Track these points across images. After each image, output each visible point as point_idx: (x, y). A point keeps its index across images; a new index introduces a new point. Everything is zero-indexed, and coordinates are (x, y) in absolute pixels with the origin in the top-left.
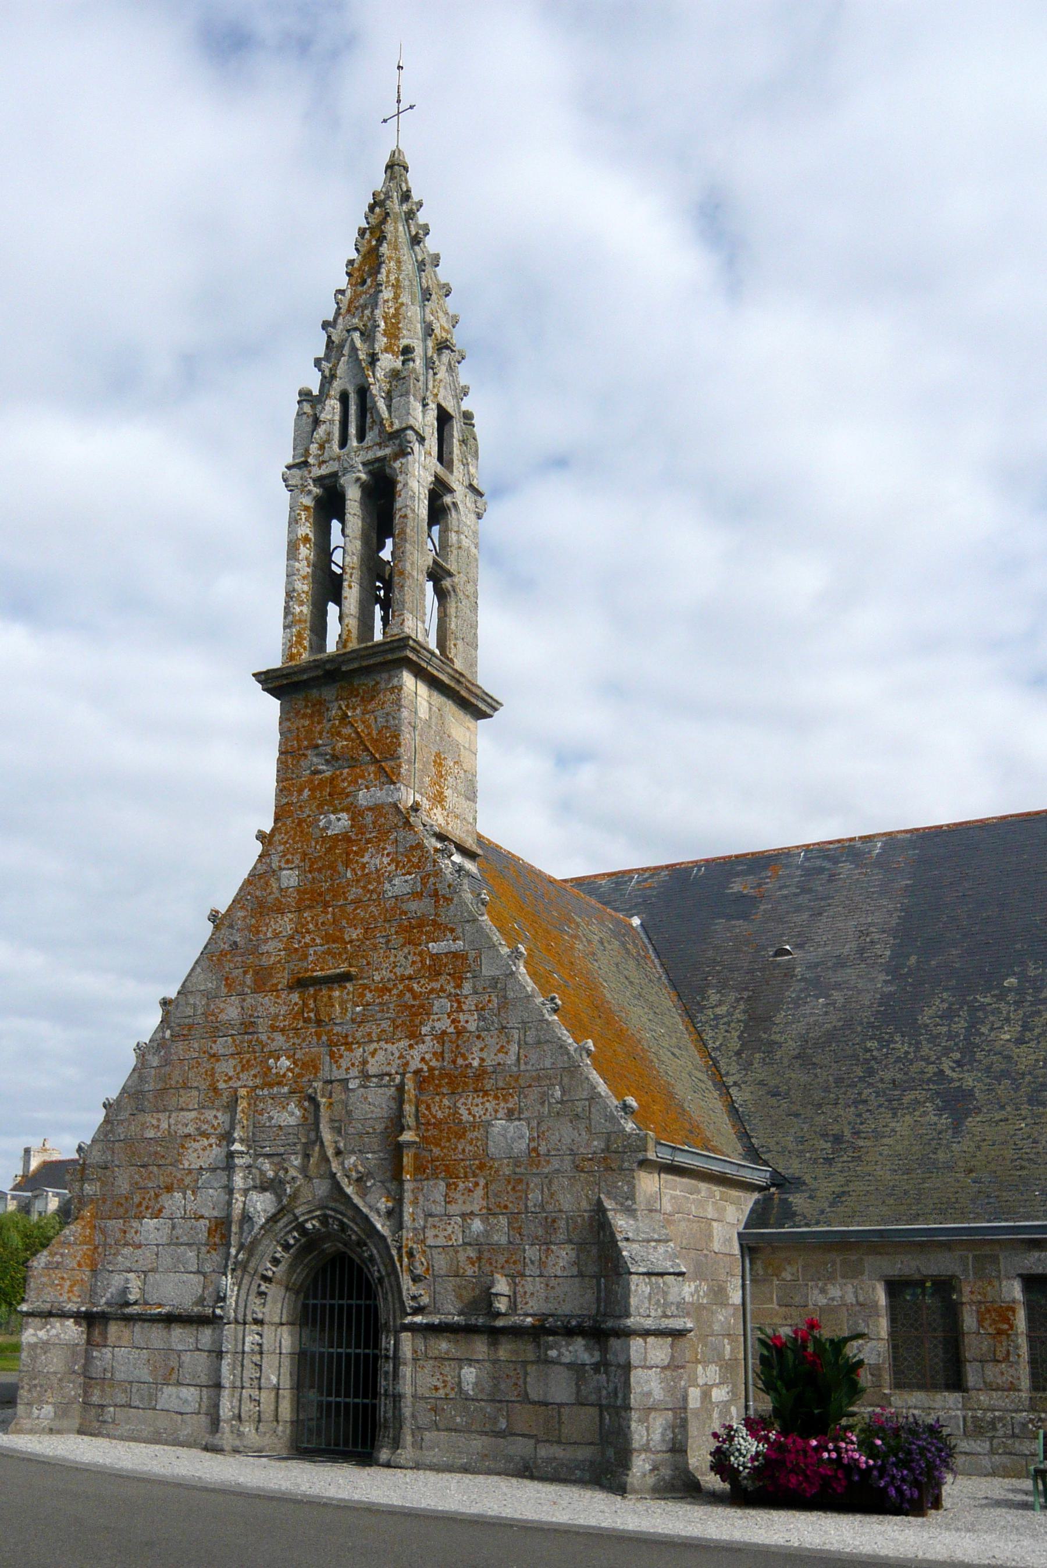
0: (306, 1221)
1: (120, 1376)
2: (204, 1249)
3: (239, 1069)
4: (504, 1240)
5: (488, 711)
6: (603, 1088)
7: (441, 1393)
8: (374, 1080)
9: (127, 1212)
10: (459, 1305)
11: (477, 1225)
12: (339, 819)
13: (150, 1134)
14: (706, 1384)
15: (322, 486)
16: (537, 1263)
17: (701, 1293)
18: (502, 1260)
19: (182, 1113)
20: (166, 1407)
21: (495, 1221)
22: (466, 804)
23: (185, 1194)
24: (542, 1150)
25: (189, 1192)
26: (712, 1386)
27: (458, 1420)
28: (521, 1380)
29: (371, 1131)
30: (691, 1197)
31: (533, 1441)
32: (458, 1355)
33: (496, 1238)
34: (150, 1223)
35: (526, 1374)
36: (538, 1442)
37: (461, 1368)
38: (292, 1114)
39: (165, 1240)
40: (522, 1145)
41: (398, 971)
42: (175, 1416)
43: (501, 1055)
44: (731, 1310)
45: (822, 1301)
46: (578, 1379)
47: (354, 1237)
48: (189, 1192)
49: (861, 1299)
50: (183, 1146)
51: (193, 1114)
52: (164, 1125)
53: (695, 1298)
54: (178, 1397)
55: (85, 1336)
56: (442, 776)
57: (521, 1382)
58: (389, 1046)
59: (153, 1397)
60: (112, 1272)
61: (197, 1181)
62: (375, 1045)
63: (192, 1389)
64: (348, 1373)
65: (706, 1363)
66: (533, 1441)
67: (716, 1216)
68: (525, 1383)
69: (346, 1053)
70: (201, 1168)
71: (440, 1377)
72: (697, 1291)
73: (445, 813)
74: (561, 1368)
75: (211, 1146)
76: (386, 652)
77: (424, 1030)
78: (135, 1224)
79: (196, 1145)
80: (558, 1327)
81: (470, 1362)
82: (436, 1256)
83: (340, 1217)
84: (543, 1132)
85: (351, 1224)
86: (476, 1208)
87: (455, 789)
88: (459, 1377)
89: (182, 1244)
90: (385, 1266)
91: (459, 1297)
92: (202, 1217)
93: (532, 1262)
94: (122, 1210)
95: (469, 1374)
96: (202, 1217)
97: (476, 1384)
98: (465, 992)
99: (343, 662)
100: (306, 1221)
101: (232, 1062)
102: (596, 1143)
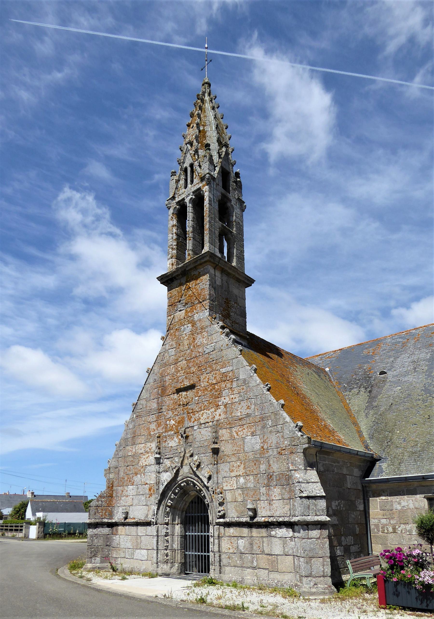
0: (182, 483)
1: (122, 546)
2: (148, 496)
3: (157, 426)
4: (252, 486)
5: (249, 283)
6: (288, 419)
7: (231, 551)
8: (203, 425)
9: (123, 483)
10: (237, 514)
11: (242, 480)
12: (188, 327)
13: (130, 454)
14: (346, 545)
15: (179, 205)
16: (265, 495)
17: (342, 506)
18: (252, 493)
19: (140, 445)
20: (137, 558)
21: (249, 478)
22: (241, 319)
23: (141, 475)
24: (265, 447)
25: (142, 474)
26: (350, 545)
27: (238, 562)
28: (261, 545)
29: (202, 445)
30: (334, 464)
31: (267, 571)
32: (237, 535)
33: (249, 485)
34: (131, 487)
35: (263, 542)
36: (269, 571)
37: (238, 540)
38: (175, 441)
39: (135, 494)
40: (258, 447)
41: (210, 381)
42: (140, 561)
43: (248, 410)
44: (358, 513)
45: (399, 507)
46: (284, 544)
47: (198, 488)
48: (142, 474)
49: (417, 506)
50: (140, 457)
51: (143, 445)
52: (134, 450)
53: (339, 507)
54: (141, 554)
55: (111, 531)
56: (229, 307)
57: (261, 546)
58: (208, 411)
59: (133, 554)
60: (119, 507)
61: (145, 470)
62: (202, 412)
63: (145, 550)
64: (189, 543)
65: (346, 536)
66: (267, 571)
67: (348, 473)
68: (263, 546)
69: (193, 416)
70: (146, 465)
71: (231, 544)
72: (339, 504)
73: (231, 322)
74: (277, 539)
75: (149, 456)
76: (201, 259)
77: (220, 403)
78: (126, 488)
79: (144, 457)
80: (274, 522)
81: (242, 537)
82: (227, 494)
83: (192, 480)
84: (265, 440)
85: (197, 483)
86: (241, 473)
87: (235, 313)
88: (238, 544)
89: (141, 495)
90: (209, 499)
91: (237, 511)
92: (147, 484)
93: (263, 494)
94: (121, 483)
95: (241, 543)
96: (147, 484)
97: (244, 547)
98: (234, 387)
99: (187, 267)
100: (182, 483)
101: (155, 423)
102: (286, 442)
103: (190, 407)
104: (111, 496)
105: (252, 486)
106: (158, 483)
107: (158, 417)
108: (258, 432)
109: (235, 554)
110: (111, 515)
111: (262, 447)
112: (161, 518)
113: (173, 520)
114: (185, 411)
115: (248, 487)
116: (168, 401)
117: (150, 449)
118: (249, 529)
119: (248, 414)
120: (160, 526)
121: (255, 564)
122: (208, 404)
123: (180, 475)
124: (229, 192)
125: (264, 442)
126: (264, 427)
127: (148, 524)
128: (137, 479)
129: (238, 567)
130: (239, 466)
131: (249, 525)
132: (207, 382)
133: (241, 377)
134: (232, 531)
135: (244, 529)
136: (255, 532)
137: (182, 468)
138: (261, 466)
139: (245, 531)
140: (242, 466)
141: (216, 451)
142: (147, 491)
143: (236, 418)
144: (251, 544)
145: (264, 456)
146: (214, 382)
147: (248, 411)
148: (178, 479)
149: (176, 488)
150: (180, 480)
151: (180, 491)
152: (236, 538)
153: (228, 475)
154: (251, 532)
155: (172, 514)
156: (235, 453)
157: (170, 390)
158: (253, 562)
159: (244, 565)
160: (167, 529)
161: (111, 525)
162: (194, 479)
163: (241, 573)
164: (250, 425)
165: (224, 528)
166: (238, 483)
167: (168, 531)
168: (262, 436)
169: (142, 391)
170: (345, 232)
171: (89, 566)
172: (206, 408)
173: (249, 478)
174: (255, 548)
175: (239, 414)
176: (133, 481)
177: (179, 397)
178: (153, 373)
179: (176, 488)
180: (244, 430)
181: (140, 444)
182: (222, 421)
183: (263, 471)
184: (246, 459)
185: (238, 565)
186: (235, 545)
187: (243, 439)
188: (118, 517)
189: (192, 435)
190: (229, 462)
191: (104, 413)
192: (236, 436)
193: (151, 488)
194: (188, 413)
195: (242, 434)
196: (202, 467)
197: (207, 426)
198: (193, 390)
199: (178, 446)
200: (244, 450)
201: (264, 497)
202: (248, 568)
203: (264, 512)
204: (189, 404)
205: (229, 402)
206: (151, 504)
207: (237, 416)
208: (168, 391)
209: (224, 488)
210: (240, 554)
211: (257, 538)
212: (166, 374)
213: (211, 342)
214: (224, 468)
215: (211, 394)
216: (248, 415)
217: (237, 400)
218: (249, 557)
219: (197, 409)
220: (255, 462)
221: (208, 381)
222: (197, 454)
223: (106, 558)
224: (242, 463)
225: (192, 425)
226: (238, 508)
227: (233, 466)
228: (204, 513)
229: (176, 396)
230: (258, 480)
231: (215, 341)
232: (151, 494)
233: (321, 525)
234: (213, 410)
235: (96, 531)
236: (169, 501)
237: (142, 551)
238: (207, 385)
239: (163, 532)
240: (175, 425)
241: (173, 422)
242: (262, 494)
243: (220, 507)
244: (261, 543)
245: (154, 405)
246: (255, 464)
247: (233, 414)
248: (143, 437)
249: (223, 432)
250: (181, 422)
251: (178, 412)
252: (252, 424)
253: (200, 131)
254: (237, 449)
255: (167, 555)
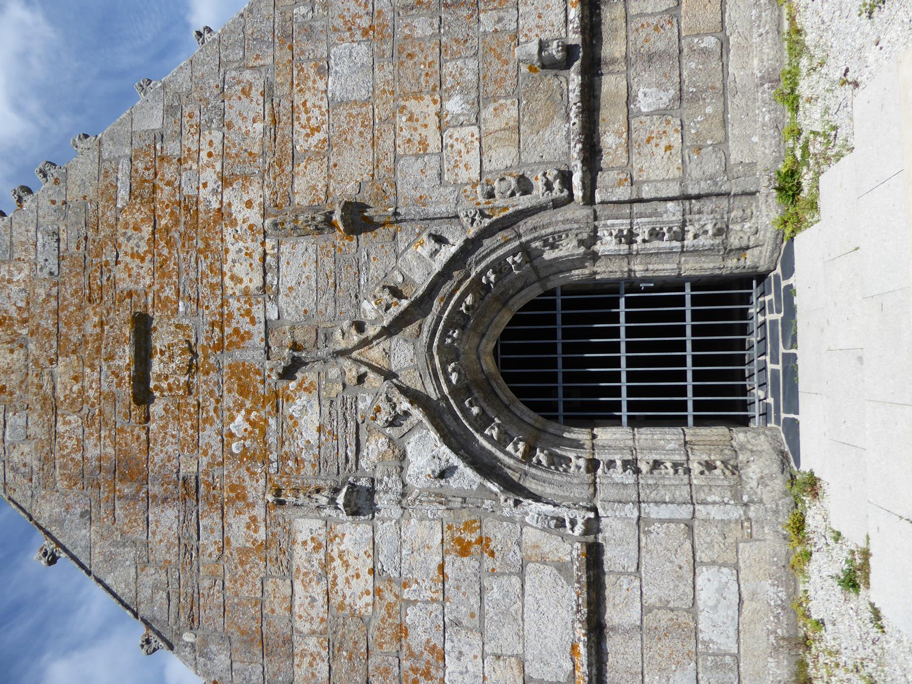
0: (448, 381)
2: (488, 563)
4: (472, 64)
7: (675, 139)
8: (269, 278)
11: (454, 105)
16: (502, 14)
19: (296, 609)
23: (409, 602)
24: (365, 22)
27: (709, 110)
29: (331, 281)
32: (622, 117)
39: (476, 639)
40: (362, 51)
51: (298, 587)
57: (653, 21)
61: (390, 580)
63: (700, 581)
68: (653, 14)
71: (653, 142)
79: (340, 581)
86: (433, 109)
93: (500, 20)
96: (441, 567)
97: (659, 86)
103: (202, 341)
105: (472, 64)
107: (211, 501)
108: (322, 51)
109: (686, 122)
111: (365, 32)
112: (569, 485)
113: (576, 445)
114: (212, 360)
115: (475, 79)
116: (167, 450)
117: (317, 548)
118: (604, 70)
119: (263, 94)
120: (600, 495)
121: (710, 42)
122: (206, 257)
123: (419, 387)
125: (350, 29)
126: (309, 32)
129: (725, 111)
130: (410, 119)
131: (592, 70)
132: (143, 260)
133: (156, 125)
134: (609, 140)
135: (605, 88)
136: (612, 48)
137: (395, 376)
138: (419, 33)
139: (611, 85)
140: (411, 104)
141: (358, 219)
142: (469, 564)
143: (267, 138)
144: (650, 58)
145: (390, 24)
146: (147, 230)
147: (255, 94)
148: (434, 397)
149: (466, 412)
150: (439, 387)
151: (476, 399)
152: (634, 123)
153: (434, 161)
154: (614, 61)
155: (558, 447)
156: (369, 136)
158: (704, 51)
159: (718, 85)
160: (611, 464)
162: (439, 318)
163: (743, 93)
164: (295, 82)
165: (601, 170)
166: (461, 118)
167: (619, 463)
168: (334, 37)
169: (107, 588)
172: (218, 264)
173: (449, 78)
174: (661, 45)
175: (259, 126)
176: (427, 656)
177: (162, 391)
178: (60, 523)
179: (466, 412)
180: (309, 104)
181: (291, 609)
182: (267, 192)
183: (432, 25)
184: (393, 92)
185: (720, 110)
186: (657, 125)
187: (334, 105)
189: (293, 328)
190: (396, 161)
192: (321, 136)
193: (460, 541)
194: (220, 347)
195: (317, 112)
196: (400, 279)
197: (273, 264)
198: (154, 324)
199: (323, 393)
200: (365, 103)
201: (507, 17)
202: (724, 67)
203: (552, 17)
204: (193, 341)
205: (218, 167)
206: (519, 544)
207: (264, 133)
208: (135, 445)
209: (475, 176)
210: (685, 105)
211: (631, 38)
212: (78, 457)
213: (32, 248)
214: (414, 182)
215: (179, 245)
216: (268, 93)
217: (217, 136)
218: (691, 64)
219: (214, 305)
220: (404, 55)
221: (139, 256)
222: (358, 305)
224: (404, 107)
225: (262, 326)
226: (540, 117)
227: (409, 141)
228: (568, 407)
229: (156, 409)
230: (457, 41)
231: (33, 229)
232: (480, 541)
234: (228, 232)
236: (510, 448)
237: (702, 596)
238: (152, 261)
240: (249, 412)
241: (239, 418)
242: (499, 27)
243: (534, 192)
244: (643, 21)
245: (167, 519)
246: (411, 56)
247: (256, 150)
248: (269, 587)
249: (303, 187)
251: (211, 393)
252: (295, 73)
254: (359, 128)
255: (709, 466)
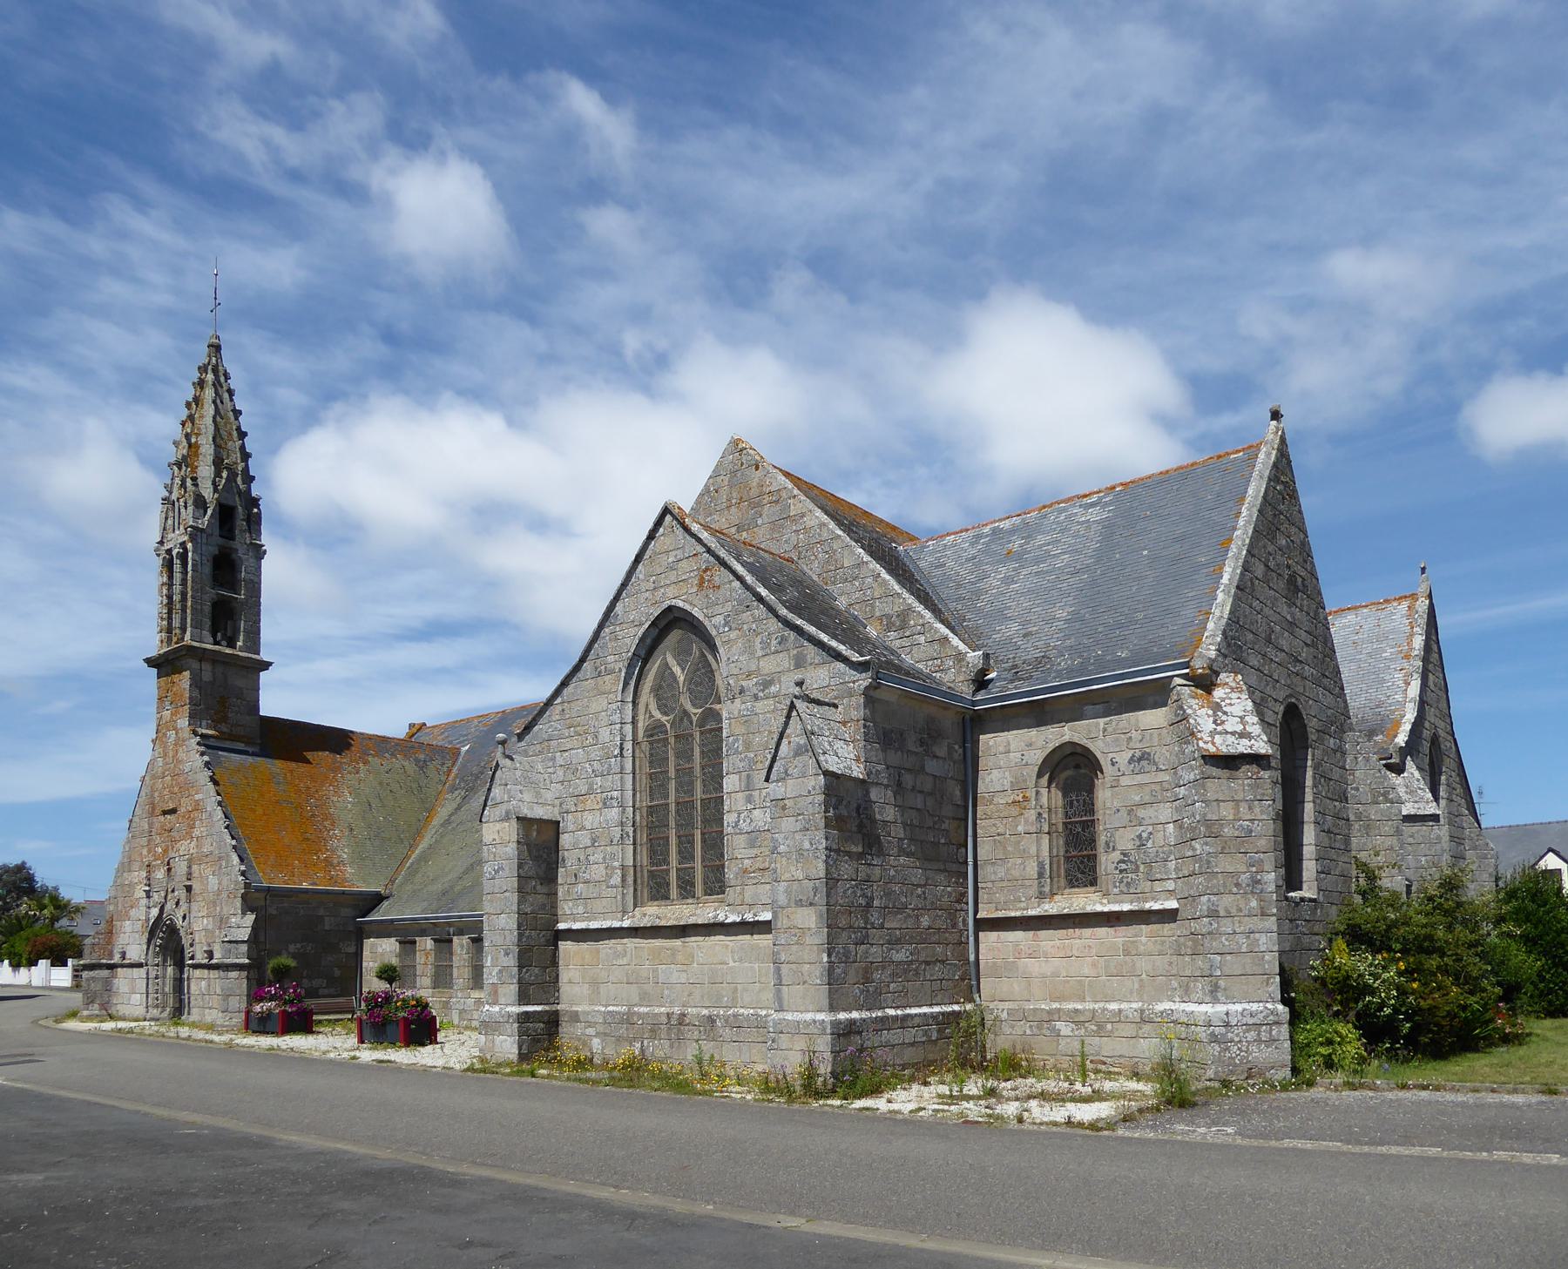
104: (111, 932)
106: (148, 920)
110: (111, 956)
113: (165, 961)
124: (233, 539)
127: (140, 965)
128: (133, 912)
141: (189, 889)
157: (158, 811)
161: (112, 967)
170: (1159, 123)
171: (85, 1013)
188: (117, 959)
191: (443, 671)
223: (105, 1006)
229: (162, 818)
233: (239, 967)
235: (92, 973)
239: (153, 974)
250: (165, 851)
253: (190, 445)
